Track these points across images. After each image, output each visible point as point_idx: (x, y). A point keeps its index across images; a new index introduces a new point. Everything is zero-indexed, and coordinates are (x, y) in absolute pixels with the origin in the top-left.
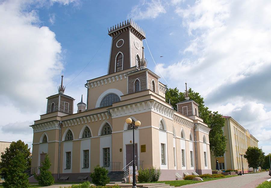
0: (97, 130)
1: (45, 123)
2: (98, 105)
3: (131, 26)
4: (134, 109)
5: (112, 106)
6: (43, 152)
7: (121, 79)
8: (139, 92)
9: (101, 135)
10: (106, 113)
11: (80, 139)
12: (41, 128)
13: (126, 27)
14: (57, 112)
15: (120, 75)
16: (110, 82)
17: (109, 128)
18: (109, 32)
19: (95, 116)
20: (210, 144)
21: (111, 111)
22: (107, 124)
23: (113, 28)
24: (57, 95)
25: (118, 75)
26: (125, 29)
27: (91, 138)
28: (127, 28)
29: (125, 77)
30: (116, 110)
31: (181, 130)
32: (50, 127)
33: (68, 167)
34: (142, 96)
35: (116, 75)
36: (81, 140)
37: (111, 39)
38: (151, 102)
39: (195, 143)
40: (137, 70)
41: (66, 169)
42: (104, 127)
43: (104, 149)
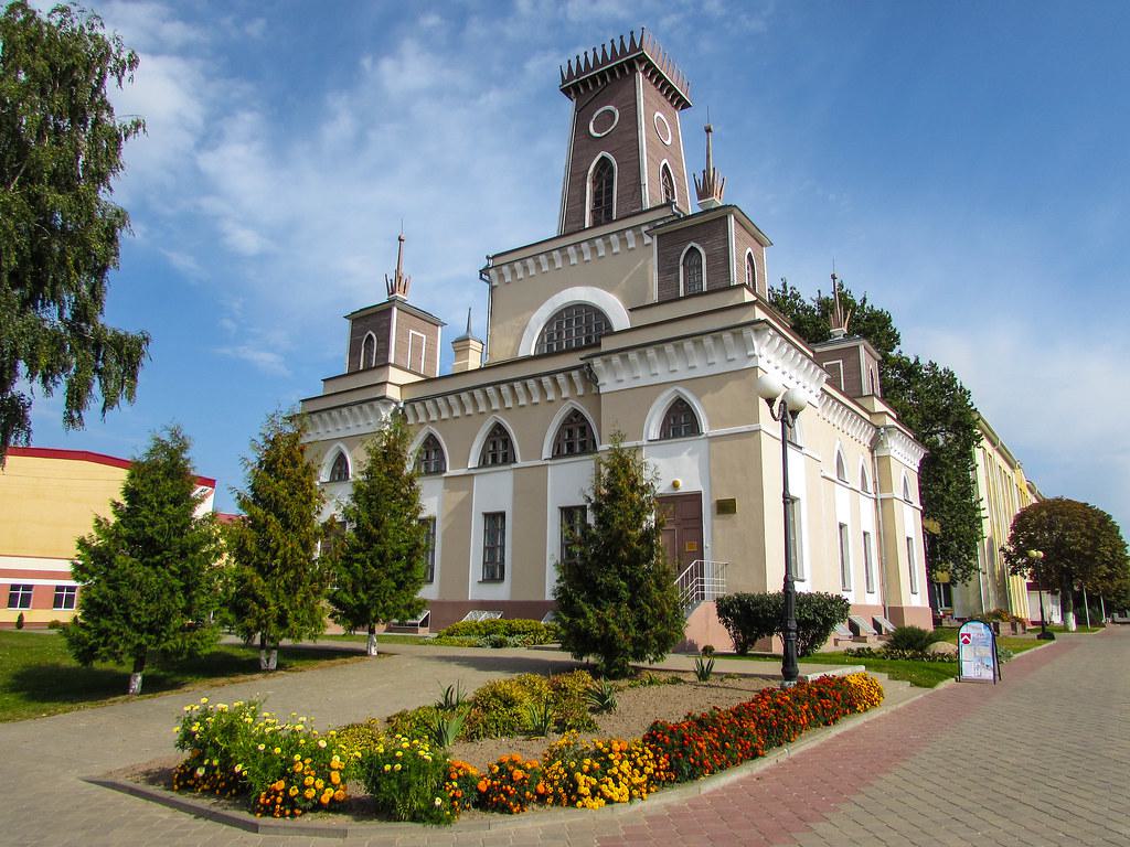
0: (536, 433)
1: (344, 406)
2: (529, 347)
3: (643, 59)
4: (686, 358)
5: (598, 345)
6: (675, 485)
7: (602, 253)
8: (679, 299)
9: (554, 458)
10: (575, 374)
11: (473, 472)
12: (366, 419)
13: (607, 69)
14: (382, 370)
15: (555, 253)
16: (574, 261)
17: (585, 428)
18: (564, 82)
19: (429, 404)
20: (921, 508)
21: (597, 363)
22: (576, 413)
23: (622, 44)
24: (385, 306)
25: (605, 237)
26: (613, 75)
27: (513, 466)
28: (631, 64)
29: (647, 240)
30: (616, 359)
31: (837, 448)
32: (320, 430)
33: (494, 573)
34: (452, 375)
35: (613, 233)
36: (472, 475)
37: (569, 107)
38: (756, 331)
39: (876, 500)
40: (675, 218)
41: (484, 581)
42: (567, 427)
43: (562, 509)
